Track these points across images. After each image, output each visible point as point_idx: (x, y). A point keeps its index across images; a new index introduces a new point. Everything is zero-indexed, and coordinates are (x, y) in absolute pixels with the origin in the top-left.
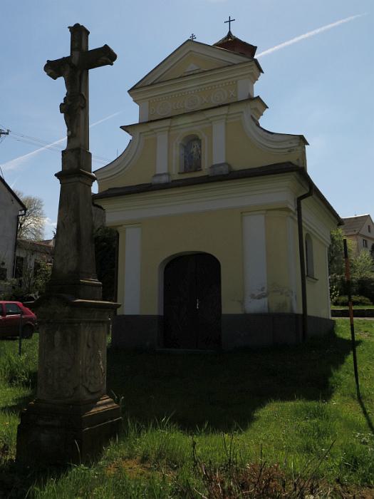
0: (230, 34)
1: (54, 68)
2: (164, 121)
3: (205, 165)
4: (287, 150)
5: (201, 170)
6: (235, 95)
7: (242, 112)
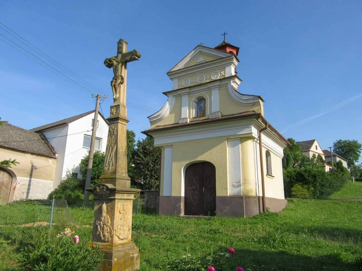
0: (224, 42)
1: (109, 64)
3: (208, 112)
4: (252, 104)
5: (205, 116)
6: (224, 75)
7: (227, 84)
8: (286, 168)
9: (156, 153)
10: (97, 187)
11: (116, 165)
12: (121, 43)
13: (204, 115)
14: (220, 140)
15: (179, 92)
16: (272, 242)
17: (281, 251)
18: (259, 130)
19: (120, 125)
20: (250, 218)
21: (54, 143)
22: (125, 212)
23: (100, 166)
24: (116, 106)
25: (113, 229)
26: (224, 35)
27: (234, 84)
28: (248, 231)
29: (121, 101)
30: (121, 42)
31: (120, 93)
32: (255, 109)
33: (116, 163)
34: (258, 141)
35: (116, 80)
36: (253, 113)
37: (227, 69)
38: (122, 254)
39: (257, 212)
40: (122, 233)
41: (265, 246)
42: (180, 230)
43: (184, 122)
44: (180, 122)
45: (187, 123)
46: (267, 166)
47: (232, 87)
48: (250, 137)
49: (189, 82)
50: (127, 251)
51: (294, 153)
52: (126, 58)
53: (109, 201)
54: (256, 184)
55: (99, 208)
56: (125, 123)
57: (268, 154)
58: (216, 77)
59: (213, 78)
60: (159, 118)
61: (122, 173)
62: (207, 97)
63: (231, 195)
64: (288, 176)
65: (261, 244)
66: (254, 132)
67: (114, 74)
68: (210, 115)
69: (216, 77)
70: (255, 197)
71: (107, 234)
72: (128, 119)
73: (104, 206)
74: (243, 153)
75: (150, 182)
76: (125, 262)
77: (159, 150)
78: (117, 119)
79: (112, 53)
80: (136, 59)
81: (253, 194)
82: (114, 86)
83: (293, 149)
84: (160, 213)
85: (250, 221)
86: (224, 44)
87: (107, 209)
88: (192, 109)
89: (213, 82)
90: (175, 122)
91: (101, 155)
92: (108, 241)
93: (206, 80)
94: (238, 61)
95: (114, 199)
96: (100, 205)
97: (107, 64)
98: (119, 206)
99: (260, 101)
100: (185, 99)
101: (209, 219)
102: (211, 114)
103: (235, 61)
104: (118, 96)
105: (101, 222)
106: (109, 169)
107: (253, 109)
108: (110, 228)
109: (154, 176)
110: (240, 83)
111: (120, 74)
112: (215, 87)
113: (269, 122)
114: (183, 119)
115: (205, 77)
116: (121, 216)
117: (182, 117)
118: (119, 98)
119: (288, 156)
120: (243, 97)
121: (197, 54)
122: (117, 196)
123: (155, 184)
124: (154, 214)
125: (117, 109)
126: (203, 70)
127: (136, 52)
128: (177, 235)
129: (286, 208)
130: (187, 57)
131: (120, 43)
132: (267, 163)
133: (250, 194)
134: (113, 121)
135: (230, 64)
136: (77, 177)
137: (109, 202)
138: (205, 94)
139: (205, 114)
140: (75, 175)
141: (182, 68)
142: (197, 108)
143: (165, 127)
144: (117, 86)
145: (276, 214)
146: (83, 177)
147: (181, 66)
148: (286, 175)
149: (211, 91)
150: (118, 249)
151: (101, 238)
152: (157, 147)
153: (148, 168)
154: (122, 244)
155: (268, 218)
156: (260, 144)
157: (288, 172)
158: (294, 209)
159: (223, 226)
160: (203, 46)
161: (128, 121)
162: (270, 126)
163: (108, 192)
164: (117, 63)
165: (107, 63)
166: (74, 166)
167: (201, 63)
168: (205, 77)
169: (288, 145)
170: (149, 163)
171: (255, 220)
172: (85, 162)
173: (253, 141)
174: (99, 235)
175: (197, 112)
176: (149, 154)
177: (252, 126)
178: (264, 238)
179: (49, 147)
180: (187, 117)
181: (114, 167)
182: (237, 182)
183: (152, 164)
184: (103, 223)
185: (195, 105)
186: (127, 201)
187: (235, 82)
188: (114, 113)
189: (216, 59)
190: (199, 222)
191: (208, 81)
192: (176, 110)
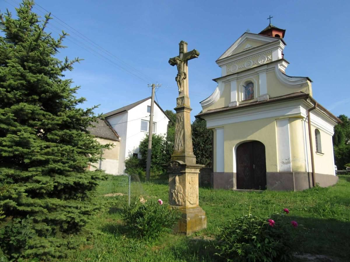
0: (270, 26)
1: (173, 62)
2: (263, 66)
3: (256, 96)
4: (300, 85)
5: (254, 99)
8: (337, 146)
9: (206, 134)
10: (171, 163)
11: (184, 146)
12: (182, 44)
13: (252, 98)
14: (269, 120)
15: (228, 78)
16: (322, 211)
17: (330, 218)
18: (308, 109)
19: (185, 113)
20: (300, 192)
21: (116, 128)
22: (193, 183)
23: (156, 147)
24: (181, 98)
25: (185, 196)
26: (270, 18)
27: (281, 67)
28: (299, 203)
29: (185, 93)
30: (182, 43)
31: (183, 87)
32: (304, 90)
33: (184, 144)
34: (307, 121)
35: (180, 76)
36: (302, 94)
37: (274, 53)
38: (193, 215)
39: (308, 187)
40: (192, 199)
41: (316, 214)
42: (237, 201)
43: (234, 105)
44: (230, 105)
45: (236, 106)
46: (317, 143)
47: (280, 70)
48: (298, 117)
49: (237, 68)
50: (197, 213)
51: (346, 130)
52: (187, 57)
53: (181, 174)
54: (305, 161)
55: (172, 180)
56: (189, 111)
57: (317, 132)
58: (264, 62)
59: (261, 63)
60: (211, 102)
61: (189, 152)
62: (254, 81)
63: (280, 171)
64: (340, 153)
65: (311, 212)
66: (303, 111)
67: (178, 71)
68: (258, 98)
69: (264, 62)
70: (304, 173)
71: (180, 200)
72: (191, 107)
73: (177, 178)
74: (292, 132)
75: (202, 161)
76: (196, 221)
77: (211, 132)
78: (183, 108)
79: (175, 53)
80: (195, 57)
81: (303, 170)
82: (179, 81)
83: (345, 126)
84: (215, 186)
85: (300, 194)
86: (270, 28)
87: (179, 180)
88: (241, 92)
89: (260, 67)
90: (225, 105)
91: (156, 137)
92: (182, 205)
93: (254, 65)
94: (285, 44)
95: (185, 173)
96: (174, 177)
97: (171, 63)
98: (189, 178)
99: (308, 82)
100: (234, 84)
101: (261, 193)
102: (259, 97)
103: (281, 45)
104: (182, 89)
105: (175, 191)
106: (179, 149)
107: (302, 90)
108: (183, 195)
109: (205, 155)
110: (287, 65)
111: (183, 71)
112: (263, 71)
113: (318, 101)
114: (233, 102)
115: (252, 63)
116: (190, 186)
117: (232, 100)
118: (183, 91)
119: (340, 133)
120: (291, 80)
121: (244, 40)
122: (187, 170)
123: (206, 162)
124: (209, 188)
125: (182, 101)
126: (250, 56)
127: (195, 51)
128: (233, 204)
129: (337, 183)
130: (235, 44)
131: (181, 44)
132: (316, 141)
133: (299, 170)
134: (179, 110)
135: (277, 48)
136: (137, 157)
137: (181, 175)
138: (253, 78)
139: (253, 97)
140: (135, 155)
141: (230, 55)
142: (246, 92)
143: (216, 111)
144: (181, 81)
145: (326, 189)
146: (143, 156)
147: (229, 53)
148: (338, 152)
149: (259, 76)
150: (190, 211)
151: (176, 202)
152: (210, 129)
153: (199, 148)
154: (193, 208)
155: (318, 192)
156: (309, 122)
157: (340, 149)
158: (346, 185)
159: (275, 198)
160: (250, 33)
161: (191, 110)
162: (319, 106)
163: (180, 167)
164: (180, 62)
165: (171, 62)
166: (134, 147)
167: (248, 49)
168: (252, 63)
169: (339, 123)
170: (199, 143)
171: (305, 193)
172: (144, 144)
173: (302, 121)
174: (175, 201)
175: (246, 96)
176: (200, 135)
177: (300, 106)
178: (314, 208)
179: (113, 131)
180: (237, 100)
181: (183, 148)
182: (286, 160)
183: (203, 144)
184: (177, 191)
185: (243, 89)
186: (194, 174)
187: (282, 65)
188: (180, 104)
189: (263, 44)
190: (252, 195)
191: (256, 66)
192: (226, 94)
